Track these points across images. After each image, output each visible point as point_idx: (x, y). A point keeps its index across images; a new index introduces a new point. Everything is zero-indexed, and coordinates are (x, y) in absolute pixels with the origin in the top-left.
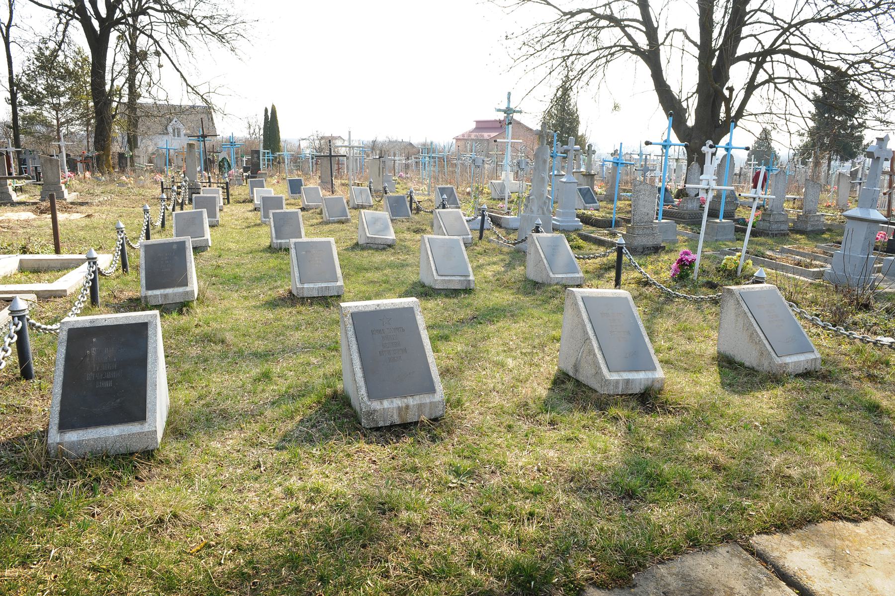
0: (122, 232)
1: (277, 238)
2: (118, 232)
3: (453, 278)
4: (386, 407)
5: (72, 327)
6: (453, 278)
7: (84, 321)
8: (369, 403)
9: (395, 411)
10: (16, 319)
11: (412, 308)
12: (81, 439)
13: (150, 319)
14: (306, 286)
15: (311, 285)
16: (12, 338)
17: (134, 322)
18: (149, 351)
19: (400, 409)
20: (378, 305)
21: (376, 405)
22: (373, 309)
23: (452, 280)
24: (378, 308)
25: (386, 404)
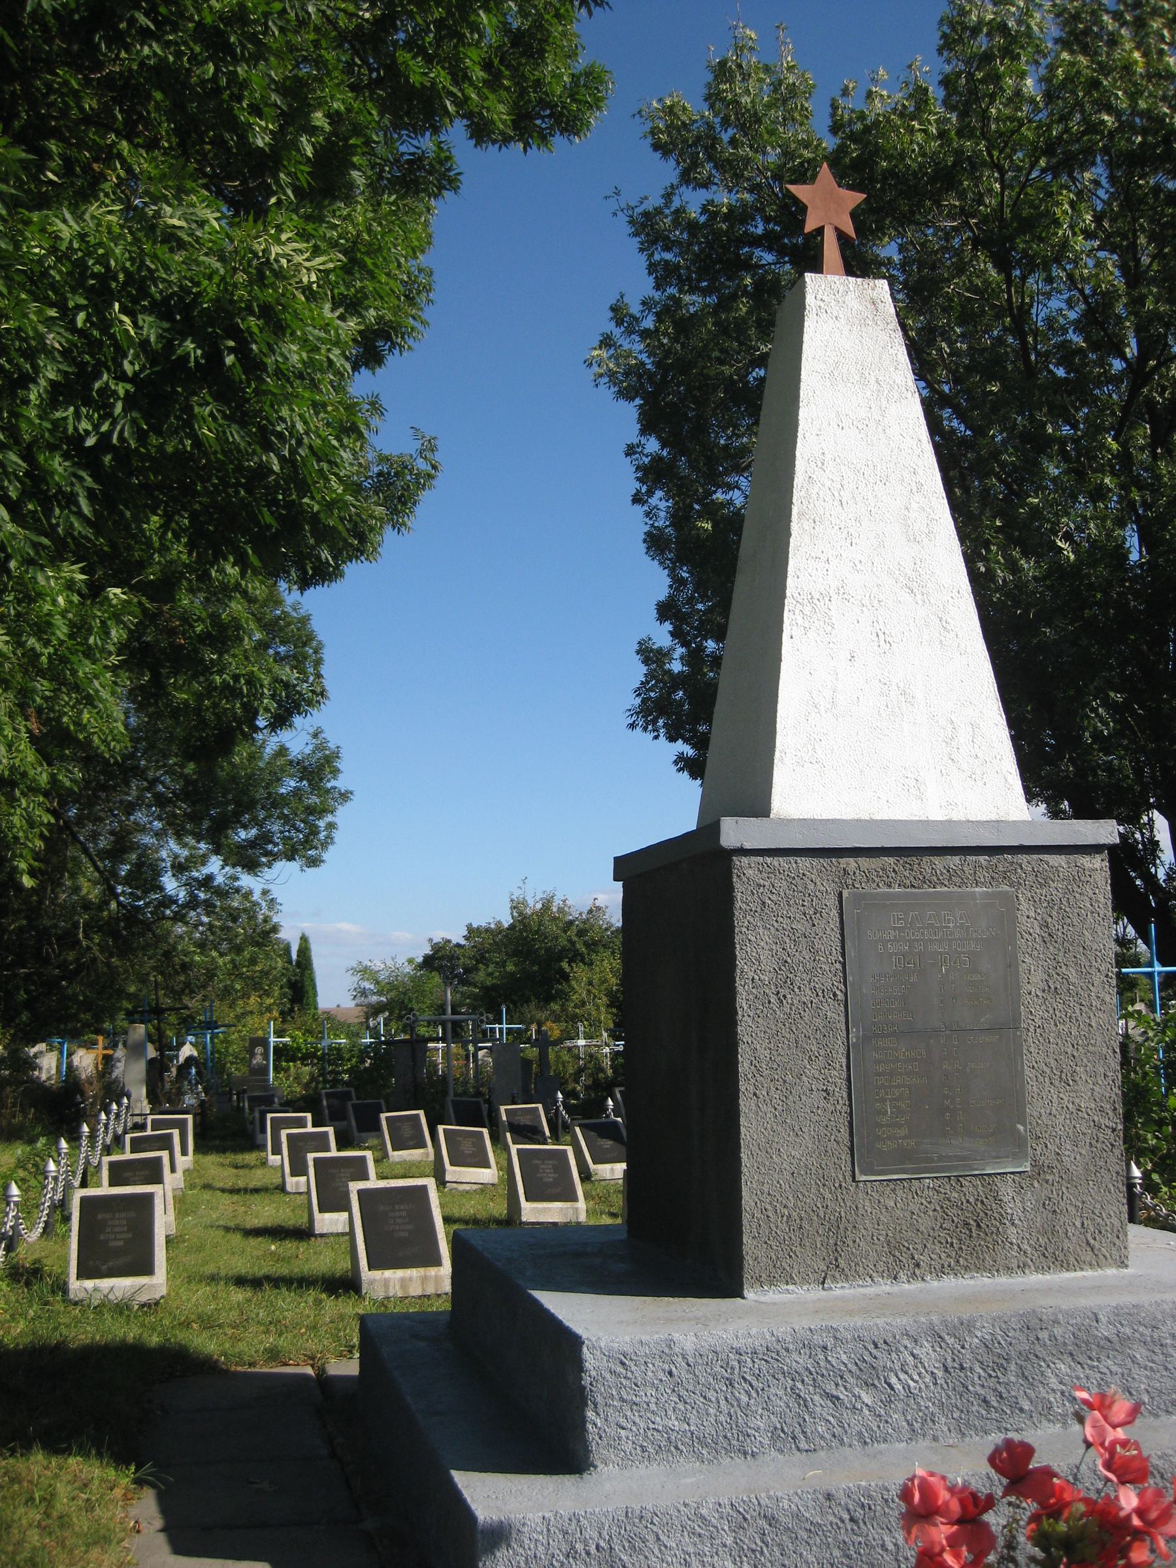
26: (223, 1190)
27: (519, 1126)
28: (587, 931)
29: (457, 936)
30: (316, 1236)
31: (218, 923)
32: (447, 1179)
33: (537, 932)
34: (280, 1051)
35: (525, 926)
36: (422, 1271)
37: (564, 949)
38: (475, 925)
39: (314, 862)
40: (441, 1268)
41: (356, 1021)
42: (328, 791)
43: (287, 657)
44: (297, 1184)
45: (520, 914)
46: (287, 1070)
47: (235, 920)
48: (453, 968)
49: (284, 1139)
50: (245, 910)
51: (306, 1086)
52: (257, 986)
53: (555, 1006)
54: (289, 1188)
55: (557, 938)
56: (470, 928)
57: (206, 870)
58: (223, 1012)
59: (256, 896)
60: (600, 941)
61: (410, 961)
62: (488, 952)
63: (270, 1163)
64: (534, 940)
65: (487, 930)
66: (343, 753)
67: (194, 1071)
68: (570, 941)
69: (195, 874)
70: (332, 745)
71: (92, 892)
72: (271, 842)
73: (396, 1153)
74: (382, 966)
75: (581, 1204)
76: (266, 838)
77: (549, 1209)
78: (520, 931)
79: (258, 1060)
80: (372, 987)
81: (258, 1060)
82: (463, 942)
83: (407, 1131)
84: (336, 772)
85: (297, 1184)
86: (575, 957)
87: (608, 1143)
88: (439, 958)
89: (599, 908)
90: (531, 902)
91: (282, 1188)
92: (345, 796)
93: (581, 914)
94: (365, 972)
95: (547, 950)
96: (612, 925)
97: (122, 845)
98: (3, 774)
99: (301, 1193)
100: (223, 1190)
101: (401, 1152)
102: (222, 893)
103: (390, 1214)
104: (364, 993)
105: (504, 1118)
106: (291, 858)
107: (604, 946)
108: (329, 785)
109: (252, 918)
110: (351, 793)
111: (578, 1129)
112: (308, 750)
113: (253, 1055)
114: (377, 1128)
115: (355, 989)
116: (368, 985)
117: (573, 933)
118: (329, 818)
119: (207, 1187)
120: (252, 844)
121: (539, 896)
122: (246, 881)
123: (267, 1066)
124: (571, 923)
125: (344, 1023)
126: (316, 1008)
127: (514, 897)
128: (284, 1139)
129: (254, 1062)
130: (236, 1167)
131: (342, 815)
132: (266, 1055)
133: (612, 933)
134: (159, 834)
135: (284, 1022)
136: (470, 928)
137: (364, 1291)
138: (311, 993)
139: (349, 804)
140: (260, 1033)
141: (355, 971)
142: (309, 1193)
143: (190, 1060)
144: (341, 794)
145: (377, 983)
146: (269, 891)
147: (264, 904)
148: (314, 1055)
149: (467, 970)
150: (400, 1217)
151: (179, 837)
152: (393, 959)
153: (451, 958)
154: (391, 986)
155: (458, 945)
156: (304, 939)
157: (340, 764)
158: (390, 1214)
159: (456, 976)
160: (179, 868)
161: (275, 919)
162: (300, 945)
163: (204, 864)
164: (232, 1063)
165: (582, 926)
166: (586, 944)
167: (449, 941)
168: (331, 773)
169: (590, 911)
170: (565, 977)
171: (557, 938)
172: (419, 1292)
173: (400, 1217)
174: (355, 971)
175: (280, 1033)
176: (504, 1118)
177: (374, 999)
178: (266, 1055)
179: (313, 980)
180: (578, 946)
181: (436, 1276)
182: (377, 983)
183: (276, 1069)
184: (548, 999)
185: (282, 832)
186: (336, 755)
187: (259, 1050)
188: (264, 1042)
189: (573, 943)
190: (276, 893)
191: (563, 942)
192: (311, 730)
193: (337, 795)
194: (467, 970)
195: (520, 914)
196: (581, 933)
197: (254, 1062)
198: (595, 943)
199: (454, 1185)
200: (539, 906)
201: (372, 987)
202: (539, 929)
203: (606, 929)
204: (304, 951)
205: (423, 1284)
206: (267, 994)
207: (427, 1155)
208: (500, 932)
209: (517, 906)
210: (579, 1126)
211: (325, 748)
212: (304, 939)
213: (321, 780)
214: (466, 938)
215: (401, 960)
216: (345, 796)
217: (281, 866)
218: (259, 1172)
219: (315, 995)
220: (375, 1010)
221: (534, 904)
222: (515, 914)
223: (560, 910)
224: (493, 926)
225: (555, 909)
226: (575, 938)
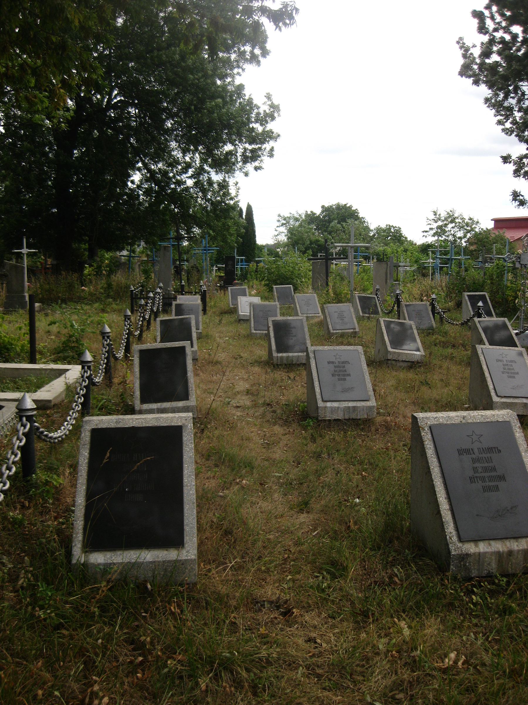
0: (108, 337)
1: (279, 351)
2: (104, 338)
3: (516, 401)
4: (482, 550)
5: (96, 427)
6: (516, 401)
7: (109, 422)
8: (460, 545)
9: (493, 558)
10: (24, 419)
11: (509, 422)
12: (109, 561)
13: (184, 421)
14: (329, 404)
15: (336, 404)
16: (21, 441)
17: (165, 425)
18: (184, 460)
19: (499, 555)
20: (464, 417)
21: (471, 548)
22: (457, 421)
23: (516, 403)
24: (464, 421)
25: (482, 547)
29: (318, 211)
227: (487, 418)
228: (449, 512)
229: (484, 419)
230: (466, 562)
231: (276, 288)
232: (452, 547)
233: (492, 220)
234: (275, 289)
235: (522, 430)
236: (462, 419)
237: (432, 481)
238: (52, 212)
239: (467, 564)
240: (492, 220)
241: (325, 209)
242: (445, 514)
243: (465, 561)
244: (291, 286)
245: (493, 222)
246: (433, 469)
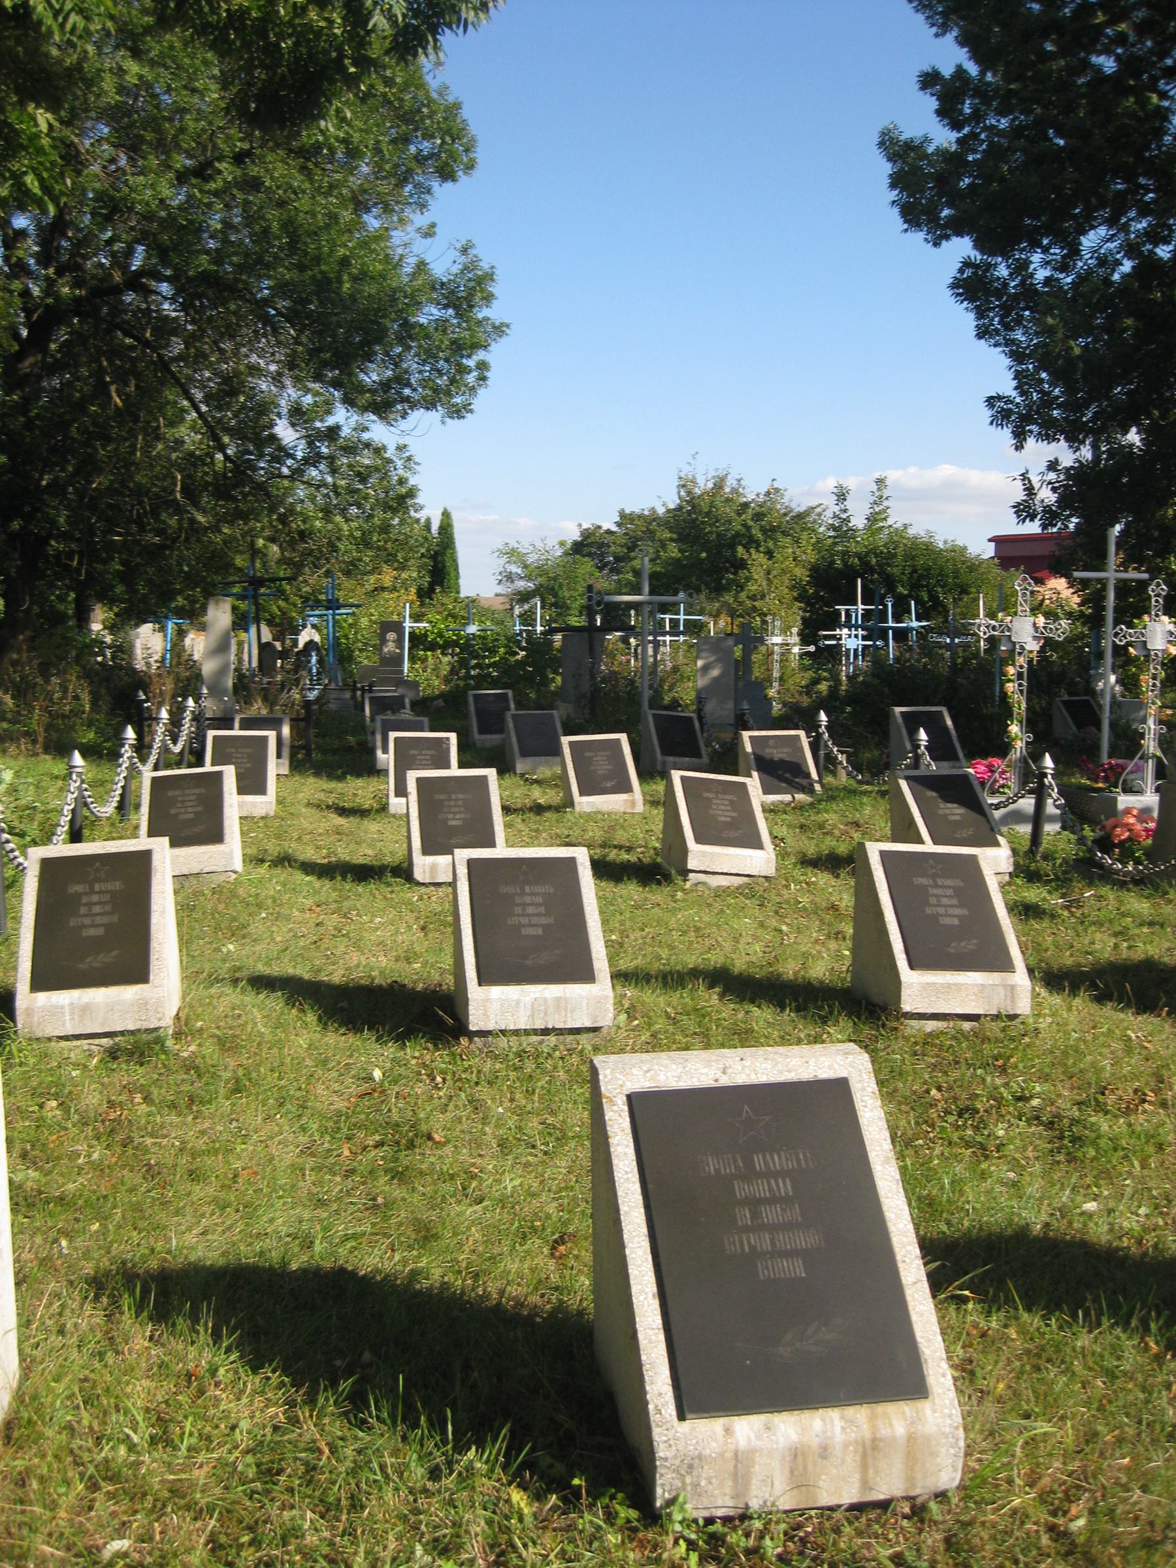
26: (308, 868)
27: (771, 761)
28: (765, 515)
29: (609, 523)
30: (471, 1035)
31: (343, 483)
32: (690, 866)
33: (708, 514)
34: (417, 639)
35: (694, 507)
36: (860, 1414)
37: (737, 535)
38: (628, 511)
39: (457, 412)
40: (925, 1406)
41: (501, 607)
42: (479, 323)
43: (431, 156)
44: (433, 868)
45: (689, 493)
46: (424, 660)
47: (363, 479)
48: (602, 555)
49: (412, 787)
50: (377, 469)
51: (447, 680)
52: (390, 558)
53: (728, 598)
54: (418, 875)
55: (730, 522)
56: (622, 515)
57: (331, 421)
58: (349, 590)
59: (390, 453)
60: (779, 527)
61: (562, 544)
62: (641, 539)
63: (392, 810)
64: (702, 522)
65: (640, 517)
66: (499, 275)
67: (314, 659)
68: (745, 525)
69: (318, 424)
70: (485, 265)
71: (190, 435)
72: (408, 385)
73: (585, 799)
74: (531, 548)
75: (1020, 977)
76: (401, 380)
77: (959, 987)
78: (689, 512)
79: (390, 647)
80: (519, 571)
81: (390, 647)
82: (614, 528)
83: (602, 765)
84: (488, 298)
85: (433, 868)
86: (751, 543)
87: (956, 811)
88: (586, 545)
89: (777, 490)
90: (701, 481)
91: (404, 872)
92: (500, 330)
93: (758, 495)
94: (512, 554)
95: (719, 535)
96: (792, 511)
97: (230, 387)
98: (1173, 1356)
99: (438, 885)
100: (308, 868)
101: (592, 799)
102: (350, 449)
103: (741, 1190)
104: (510, 577)
105: (749, 749)
106: (430, 405)
107: (783, 532)
108: (480, 316)
109: (385, 476)
110: (508, 326)
111: (903, 784)
112: (456, 269)
113: (384, 641)
114: (556, 751)
115: (501, 573)
116: (515, 569)
117: (747, 516)
118: (481, 355)
119: (284, 860)
120: (385, 385)
121: (712, 473)
122: (379, 432)
123: (401, 656)
124: (746, 505)
125: (487, 610)
126: (458, 592)
127: (682, 475)
128: (412, 787)
129: (386, 650)
130: (343, 812)
131: (496, 354)
132: (399, 642)
133: (793, 518)
134: (277, 379)
135: (422, 605)
136: (622, 515)
137: (661, 1495)
138: (453, 574)
139: (504, 340)
140: (395, 618)
141: (502, 553)
142: (453, 884)
143: (310, 644)
144: (494, 327)
145: (525, 567)
146: (405, 446)
147: (399, 463)
148: (455, 644)
149: (618, 559)
150: (772, 1200)
151: (297, 380)
152: (542, 540)
153: (601, 545)
154: (541, 570)
155: (609, 532)
156: (446, 515)
157: (494, 289)
158: (741, 1190)
159: (606, 565)
160: (297, 414)
161: (412, 481)
162: (442, 521)
163: (329, 412)
164: (361, 650)
165: (758, 509)
166: (764, 531)
167: (600, 527)
168: (483, 298)
169: (768, 493)
170: (742, 565)
171: (730, 522)
172: (850, 1495)
173: (772, 1200)
174: (502, 553)
175: (417, 618)
176: (749, 749)
177: (521, 585)
178: (399, 642)
179: (455, 561)
180: (754, 532)
181: (911, 1439)
182: (525, 567)
183: (413, 659)
184: (718, 589)
185: (420, 372)
186: (489, 277)
187: (391, 636)
188: (398, 627)
189: (748, 528)
190: (413, 450)
191: (737, 526)
192: (459, 246)
193: (489, 329)
194: (618, 559)
195: (689, 493)
196: (758, 516)
197: (386, 650)
198: (773, 529)
199: (702, 877)
200: (710, 485)
201: (519, 571)
202: (710, 511)
203: (785, 515)
204: (446, 527)
205: (864, 1467)
206: (403, 567)
207: (633, 803)
208: (654, 520)
209: (685, 484)
210: (907, 778)
211: (476, 268)
212: (446, 515)
213: (471, 306)
214: (619, 525)
215: (552, 542)
216: (500, 330)
217: (418, 416)
218: (372, 827)
219: (457, 577)
220: (524, 597)
221: (704, 484)
222: (683, 493)
223: (735, 491)
224: (646, 513)
225: (727, 490)
226: (751, 523)
227: (789, 1071)
228: (661, 1337)
229: (781, 1072)
230: (699, 1476)
231: (571, 744)
232: (660, 1434)
233: (990, 540)
234: (567, 751)
235: (879, 1102)
236: (719, 1074)
237: (622, 1246)
238: (1119, 522)
239: (703, 1483)
240: (990, 540)
241: (625, 518)
242: (650, 1341)
243: (695, 1473)
244: (623, 737)
245: (993, 544)
246: (626, 1213)
